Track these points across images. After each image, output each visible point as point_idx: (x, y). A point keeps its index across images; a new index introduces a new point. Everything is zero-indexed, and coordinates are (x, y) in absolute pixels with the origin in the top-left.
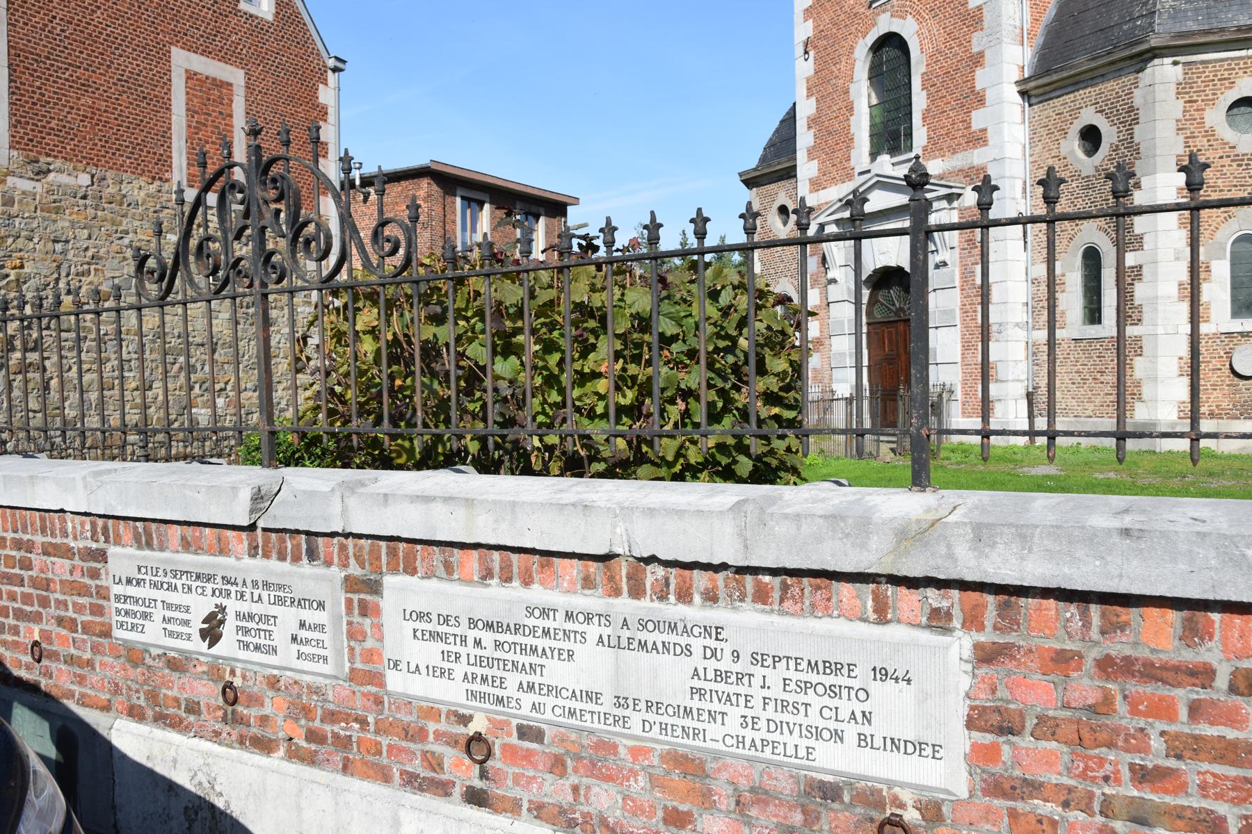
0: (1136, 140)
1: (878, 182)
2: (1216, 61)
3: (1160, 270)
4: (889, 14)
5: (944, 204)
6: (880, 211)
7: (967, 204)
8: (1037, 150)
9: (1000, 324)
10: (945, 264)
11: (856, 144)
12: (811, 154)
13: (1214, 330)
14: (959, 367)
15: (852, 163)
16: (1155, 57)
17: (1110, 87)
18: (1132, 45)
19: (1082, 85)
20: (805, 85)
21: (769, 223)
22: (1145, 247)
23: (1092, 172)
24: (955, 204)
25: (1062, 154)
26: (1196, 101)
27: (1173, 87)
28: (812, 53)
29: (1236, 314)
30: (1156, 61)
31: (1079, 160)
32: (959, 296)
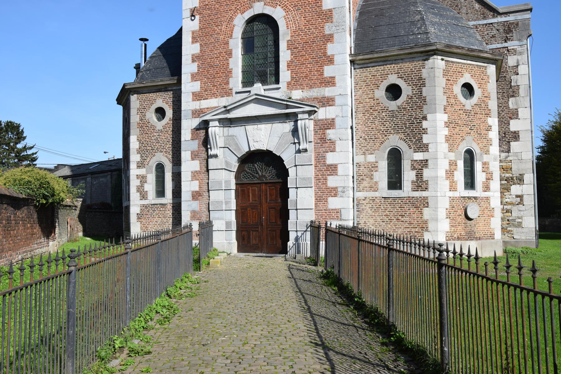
5: (306, 116)
6: (255, 116)
8: (359, 93)
9: (344, 188)
11: (233, 75)
12: (194, 77)
13: (458, 196)
15: (231, 86)
16: (435, 54)
17: (407, 66)
18: (426, 46)
19: (389, 63)
21: (147, 117)
22: (430, 150)
24: (312, 117)
25: (376, 97)
26: (450, 80)
27: (442, 71)
28: (197, 17)
30: (435, 57)
31: (153, 121)
32: (314, 170)
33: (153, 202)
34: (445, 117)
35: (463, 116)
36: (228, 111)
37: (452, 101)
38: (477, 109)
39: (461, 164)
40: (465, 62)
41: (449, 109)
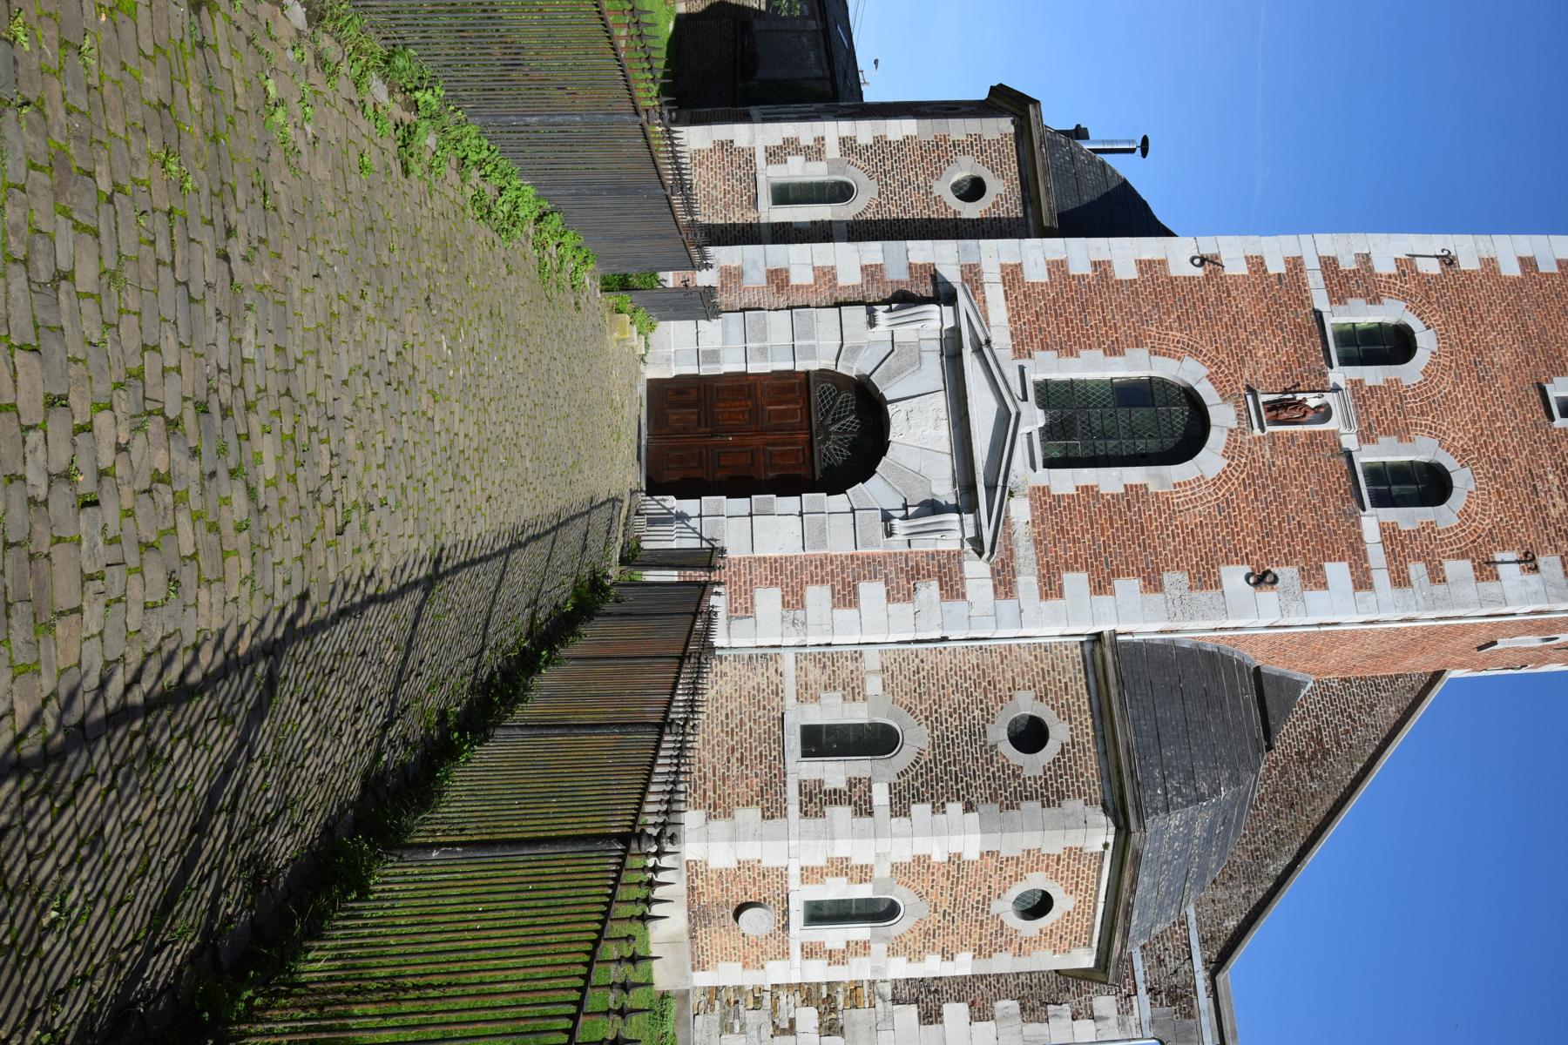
0: (1025, 805)
2: (1098, 884)
4: (1234, 425)
6: (967, 414)
9: (804, 624)
12: (1057, 268)
14: (747, 553)
15: (1038, 354)
16: (1118, 828)
17: (1090, 766)
20: (1157, 257)
21: (961, 158)
22: (895, 820)
23: (990, 740)
24: (968, 547)
28: (1200, 272)
30: (1112, 829)
32: (844, 553)
33: (761, 178)
35: (975, 896)
36: (978, 349)
38: (992, 928)
39: (864, 892)
40: (1102, 898)
41: (992, 862)
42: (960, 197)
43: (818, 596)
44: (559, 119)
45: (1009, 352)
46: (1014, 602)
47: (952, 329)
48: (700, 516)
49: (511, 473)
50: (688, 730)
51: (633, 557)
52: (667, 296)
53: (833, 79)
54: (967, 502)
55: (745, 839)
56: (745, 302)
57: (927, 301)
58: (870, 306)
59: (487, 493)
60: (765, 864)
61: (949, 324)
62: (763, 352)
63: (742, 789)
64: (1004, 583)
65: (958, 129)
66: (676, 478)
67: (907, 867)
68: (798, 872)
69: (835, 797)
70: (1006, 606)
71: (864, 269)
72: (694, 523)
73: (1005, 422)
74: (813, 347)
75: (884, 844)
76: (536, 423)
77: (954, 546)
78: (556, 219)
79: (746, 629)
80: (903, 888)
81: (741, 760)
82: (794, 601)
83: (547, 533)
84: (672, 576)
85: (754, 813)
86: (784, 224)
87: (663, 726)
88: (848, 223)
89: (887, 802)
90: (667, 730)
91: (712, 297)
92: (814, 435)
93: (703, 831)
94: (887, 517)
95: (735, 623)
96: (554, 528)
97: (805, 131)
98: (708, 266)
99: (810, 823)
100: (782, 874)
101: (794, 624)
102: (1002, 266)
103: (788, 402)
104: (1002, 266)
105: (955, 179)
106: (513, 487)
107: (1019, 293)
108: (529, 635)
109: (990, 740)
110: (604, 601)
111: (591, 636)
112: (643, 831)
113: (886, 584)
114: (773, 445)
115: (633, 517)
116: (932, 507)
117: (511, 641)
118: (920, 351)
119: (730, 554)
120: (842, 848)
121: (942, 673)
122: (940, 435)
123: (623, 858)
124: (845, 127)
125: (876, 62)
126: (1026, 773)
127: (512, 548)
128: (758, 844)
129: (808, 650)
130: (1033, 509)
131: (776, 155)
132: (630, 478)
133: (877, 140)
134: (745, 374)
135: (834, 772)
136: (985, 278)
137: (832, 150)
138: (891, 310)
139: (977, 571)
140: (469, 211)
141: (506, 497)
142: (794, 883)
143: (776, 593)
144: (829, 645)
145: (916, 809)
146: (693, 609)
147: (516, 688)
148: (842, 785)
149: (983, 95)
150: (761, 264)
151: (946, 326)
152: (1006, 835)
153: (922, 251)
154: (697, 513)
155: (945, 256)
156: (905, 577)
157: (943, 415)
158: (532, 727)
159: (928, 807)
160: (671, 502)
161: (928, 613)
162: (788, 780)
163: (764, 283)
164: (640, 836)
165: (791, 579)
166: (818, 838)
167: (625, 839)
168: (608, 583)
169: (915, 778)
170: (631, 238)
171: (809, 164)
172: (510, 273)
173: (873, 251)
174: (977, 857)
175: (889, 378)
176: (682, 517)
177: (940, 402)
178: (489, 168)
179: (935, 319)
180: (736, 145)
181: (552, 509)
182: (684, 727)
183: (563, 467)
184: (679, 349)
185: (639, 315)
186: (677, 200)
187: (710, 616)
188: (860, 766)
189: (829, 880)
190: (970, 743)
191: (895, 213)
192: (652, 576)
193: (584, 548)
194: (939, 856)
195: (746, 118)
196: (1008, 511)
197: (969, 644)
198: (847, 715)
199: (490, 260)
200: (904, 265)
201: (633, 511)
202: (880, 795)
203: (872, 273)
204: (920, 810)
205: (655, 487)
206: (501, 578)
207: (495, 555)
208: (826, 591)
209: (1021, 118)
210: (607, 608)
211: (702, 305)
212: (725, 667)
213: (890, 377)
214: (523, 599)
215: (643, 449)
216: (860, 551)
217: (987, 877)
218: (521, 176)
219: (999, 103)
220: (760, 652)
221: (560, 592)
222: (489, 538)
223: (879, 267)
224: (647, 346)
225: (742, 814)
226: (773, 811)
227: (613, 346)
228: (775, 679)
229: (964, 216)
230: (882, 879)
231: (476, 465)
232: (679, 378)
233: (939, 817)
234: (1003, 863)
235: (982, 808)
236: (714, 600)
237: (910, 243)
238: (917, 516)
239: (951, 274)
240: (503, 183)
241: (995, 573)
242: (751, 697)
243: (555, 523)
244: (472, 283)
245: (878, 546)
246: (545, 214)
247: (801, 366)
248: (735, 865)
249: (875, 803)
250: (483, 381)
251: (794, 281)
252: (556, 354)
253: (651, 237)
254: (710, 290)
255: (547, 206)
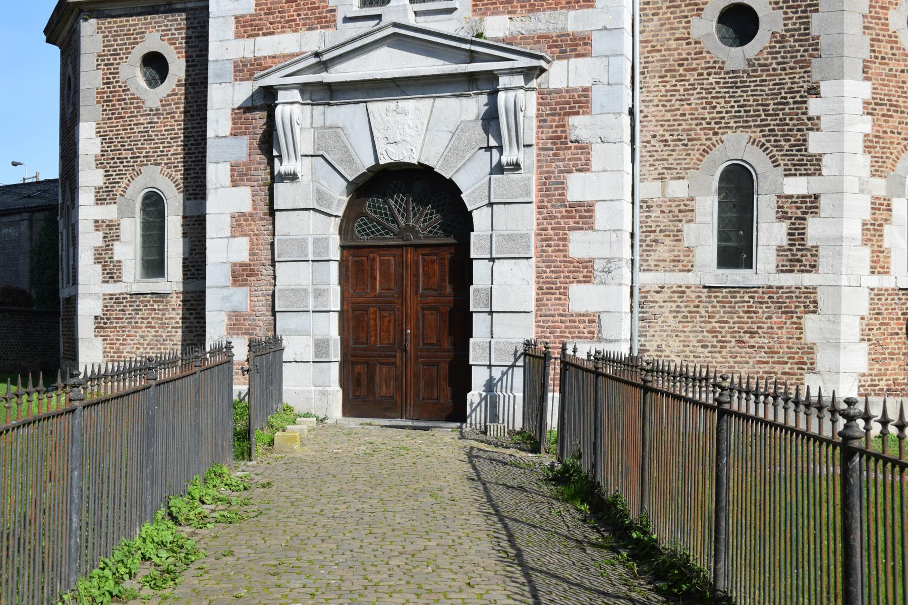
0: (814, 31)
1: (395, 34)
3: (845, 202)
5: (519, 80)
6: (393, 80)
7: (553, 86)
9: (609, 261)
10: (516, 167)
21: (122, 77)
22: (824, 171)
23: (743, 66)
24: (534, 83)
29: (751, 268)
31: (138, 86)
32: (535, 216)
33: (135, 289)
34: (865, 90)
36: (325, 66)
37: (885, 48)
41: (875, 68)
42: (163, 79)
43: (579, 245)
44: (76, 493)
45: (329, 32)
46: (595, 37)
47: (302, 92)
48: (490, 366)
49: (443, 561)
50: (727, 384)
51: (532, 440)
52: (258, 392)
53: (31, 210)
54: (487, 83)
55: (838, 332)
56: (265, 310)
57: (271, 118)
58: (275, 178)
59: (464, 587)
60: (865, 312)
61: (296, 95)
62: (319, 293)
63: (783, 334)
64: (574, 46)
65: (90, 79)
66: (448, 391)
67: (876, 160)
68: (876, 277)
69: (797, 234)
70: (599, 44)
71: (235, 184)
72: (497, 373)
73: (402, 39)
74: (316, 241)
75: (850, 184)
76: (390, 533)
77: (533, 97)
78: (178, 504)
79: (612, 321)
80: (899, 165)
81: (752, 333)
82: (584, 271)
83: (506, 527)
84: (553, 399)
85: (810, 321)
86: (185, 266)
87: (723, 412)
88: (187, 199)
89: (805, 178)
90: (726, 406)
91: (259, 343)
92: (412, 238)
93: (827, 377)
94: (499, 169)
95: (605, 334)
96: (501, 519)
97: (88, 241)
98: (229, 346)
99: (824, 262)
100: (877, 294)
101: (609, 272)
102: (238, 36)
103: (373, 269)
104: (238, 36)
105: (143, 84)
106: (458, 560)
107: (266, 20)
108: (614, 550)
109: (743, 66)
110: (578, 471)
111: (615, 484)
112: (840, 434)
113: (570, 172)
114: (417, 287)
115: (488, 437)
116: (490, 120)
117: (621, 570)
118: (324, 127)
119: (532, 336)
120: (852, 229)
121: (668, 116)
122: (414, 109)
123: (869, 455)
124: (85, 198)
125: (15, 164)
126: (780, 28)
127: (522, 564)
128: (844, 319)
129: (637, 258)
130: (496, 13)
131: (112, 272)
132: (447, 439)
133: (100, 165)
134: (341, 313)
135: (769, 234)
136: (249, 55)
137: (109, 212)
138: (280, 157)
139: (561, 75)
140: (167, 592)
141: (469, 568)
142: (887, 282)
143: (575, 289)
144: (632, 235)
145: (813, 149)
146: (592, 376)
147: (673, 566)
148: (783, 228)
149: (55, 51)
150: (225, 292)
151: (299, 99)
152: (846, 52)
153: (219, 122)
154: (486, 371)
155: (225, 97)
156: (565, 151)
157: (392, 105)
158: (717, 550)
159: (811, 136)
160: (474, 396)
161: (603, 129)
162: (775, 283)
163: (247, 289)
164: (846, 437)
165: (559, 273)
166: (840, 254)
167: (848, 453)
168: (559, 466)
169: (780, 148)
170: (198, 425)
171: (122, 238)
172: (232, 553)
173: (217, 173)
174: (868, 84)
175: (351, 161)
176: (490, 386)
177: (378, 108)
178: (123, 570)
179: (291, 111)
180: (99, 313)
181: (480, 520)
182: (723, 389)
183: (436, 507)
184: (312, 383)
185: (276, 422)
186: (162, 375)
187: (602, 358)
188: (765, 207)
189: (886, 244)
190: (744, 87)
191: (176, 149)
192: (552, 420)
193: (521, 488)
194: (866, 125)
195: (72, 302)
196: (497, 39)
197: (637, 85)
198: (708, 219)
199: (218, 573)
200: (232, 140)
201: (482, 437)
202: (797, 186)
203: (239, 176)
204: (815, 143)
205: (457, 413)
206: (554, 576)
207: (530, 582)
208: (574, 236)
209: (81, 11)
210: (586, 468)
211: (267, 354)
212: (651, 346)
213: (350, 160)
214: (577, 554)
215: (417, 424)
216: (534, 199)
217: (891, 74)
218: (131, 537)
219: (64, 33)
220: (636, 309)
221: (569, 517)
222: (512, 587)
223: (234, 167)
224: (308, 415)
225: (810, 336)
226: (808, 302)
227: (308, 451)
228: (666, 294)
229: (183, 75)
230: (888, 186)
231: (434, 597)
232: (343, 384)
233: (823, 124)
234: (877, 56)
235: (815, 77)
236: (582, 354)
237: (210, 134)
238: (498, 137)
239: (244, 91)
240: (138, 555)
241: (563, 55)
242: (685, 320)
243: (495, 518)
244: (243, 592)
245: (529, 179)
246: (170, 514)
247: (335, 253)
248: (865, 344)
249: (804, 192)
250: (346, 586)
251: (245, 257)
252: (317, 510)
253: (197, 405)
254: (252, 345)
255: (162, 512)
